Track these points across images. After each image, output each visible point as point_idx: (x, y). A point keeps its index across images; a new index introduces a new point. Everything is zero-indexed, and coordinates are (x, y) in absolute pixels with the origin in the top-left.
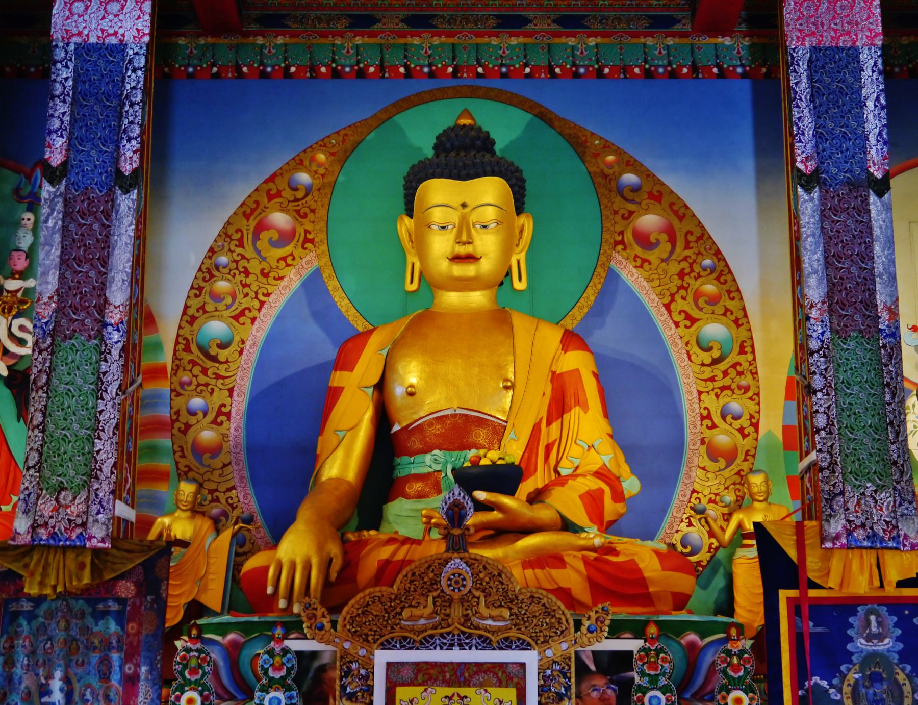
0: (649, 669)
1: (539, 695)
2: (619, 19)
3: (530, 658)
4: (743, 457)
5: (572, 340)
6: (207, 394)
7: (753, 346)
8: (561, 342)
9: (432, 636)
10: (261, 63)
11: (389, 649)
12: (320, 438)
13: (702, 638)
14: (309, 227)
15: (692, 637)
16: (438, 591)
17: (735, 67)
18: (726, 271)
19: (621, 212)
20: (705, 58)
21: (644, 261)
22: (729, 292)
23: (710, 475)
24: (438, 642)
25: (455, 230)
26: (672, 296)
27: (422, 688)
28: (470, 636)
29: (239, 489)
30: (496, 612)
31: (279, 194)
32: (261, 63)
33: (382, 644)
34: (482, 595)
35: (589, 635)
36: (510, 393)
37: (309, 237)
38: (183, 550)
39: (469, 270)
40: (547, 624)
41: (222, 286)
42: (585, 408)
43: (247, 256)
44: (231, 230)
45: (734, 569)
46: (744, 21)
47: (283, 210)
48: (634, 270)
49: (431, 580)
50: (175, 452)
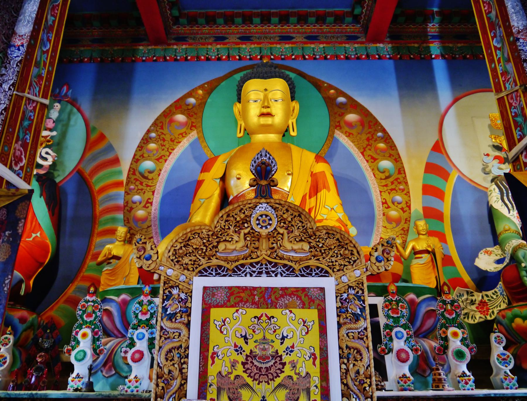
0: (393, 313)
1: (338, 316)
2: (333, 37)
3: (329, 284)
4: (404, 221)
5: (319, 158)
6: (142, 194)
7: (404, 171)
8: (315, 158)
9: (243, 265)
10: (175, 55)
11: (206, 276)
12: (192, 205)
13: (418, 296)
14: (194, 120)
15: (412, 296)
16: (249, 229)
17: (386, 55)
18: (389, 138)
19: (338, 113)
20: (372, 52)
21: (350, 134)
22: (391, 147)
23: (389, 230)
24: (248, 270)
25: (261, 102)
26: (364, 149)
27: (234, 309)
28: (276, 265)
29: (155, 238)
30: (297, 246)
31: (180, 107)
32: (175, 55)
33: (200, 272)
34: (286, 231)
35: (377, 264)
36: (290, 177)
37: (194, 124)
38: (117, 261)
39: (268, 121)
40: (341, 255)
41: (152, 146)
42: (329, 190)
43: (164, 132)
44: (158, 122)
45: (412, 270)
46: (389, 37)
47: (182, 113)
48: (346, 138)
49: (242, 219)
50: (124, 221)
